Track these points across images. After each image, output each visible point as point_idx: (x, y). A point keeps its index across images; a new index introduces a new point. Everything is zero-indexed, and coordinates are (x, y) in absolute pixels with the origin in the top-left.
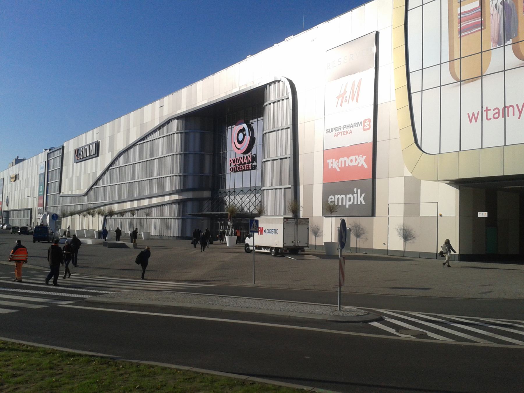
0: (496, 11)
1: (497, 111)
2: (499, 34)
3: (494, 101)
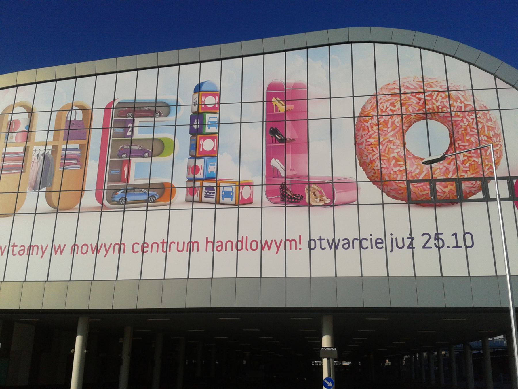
0: (36, 160)
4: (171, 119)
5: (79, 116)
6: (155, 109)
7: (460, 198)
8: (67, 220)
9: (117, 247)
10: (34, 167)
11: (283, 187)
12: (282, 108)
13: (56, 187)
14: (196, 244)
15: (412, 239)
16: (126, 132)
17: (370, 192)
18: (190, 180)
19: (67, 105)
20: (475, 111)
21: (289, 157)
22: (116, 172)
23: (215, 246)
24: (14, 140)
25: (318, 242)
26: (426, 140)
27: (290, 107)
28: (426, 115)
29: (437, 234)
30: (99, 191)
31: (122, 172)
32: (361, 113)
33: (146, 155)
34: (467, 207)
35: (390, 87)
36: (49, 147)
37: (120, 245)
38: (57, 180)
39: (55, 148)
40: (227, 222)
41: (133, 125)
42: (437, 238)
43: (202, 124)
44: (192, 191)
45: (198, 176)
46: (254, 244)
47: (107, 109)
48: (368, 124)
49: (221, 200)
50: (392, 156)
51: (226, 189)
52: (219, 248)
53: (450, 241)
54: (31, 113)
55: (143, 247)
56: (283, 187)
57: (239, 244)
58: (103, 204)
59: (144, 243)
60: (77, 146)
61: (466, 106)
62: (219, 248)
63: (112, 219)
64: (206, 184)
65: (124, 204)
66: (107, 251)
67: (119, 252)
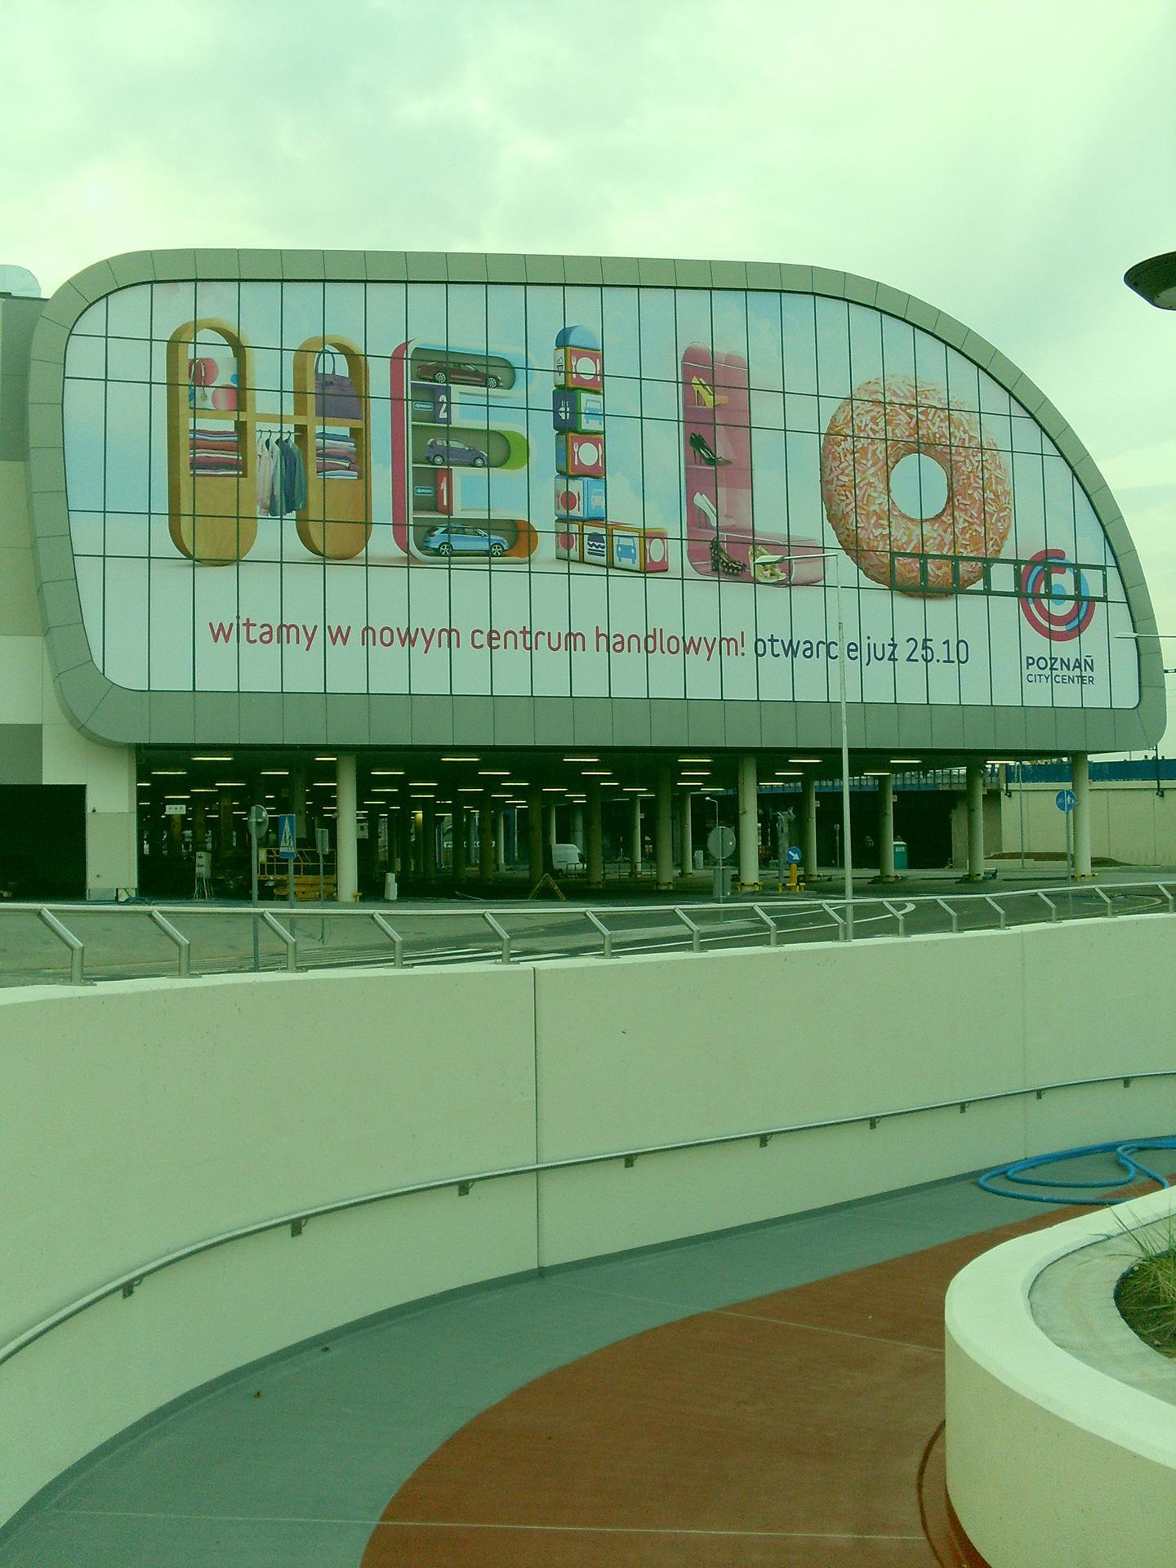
0: (266, 453)
1: (267, 629)
2: (272, 496)
3: (551, 622)
4: (516, 395)
5: (342, 368)
6: (485, 372)
7: (954, 588)
8: (345, 579)
9: (445, 635)
10: (265, 468)
11: (715, 545)
12: (708, 399)
13: (314, 513)
14: (579, 638)
15: (894, 646)
16: (436, 412)
17: (842, 568)
18: (560, 520)
19: (311, 341)
20: (981, 449)
21: (722, 492)
22: (428, 491)
23: (612, 643)
24: (209, 404)
25: (768, 644)
26: (917, 487)
27: (722, 399)
28: (921, 446)
29: (925, 640)
30: (399, 525)
31: (438, 493)
32: (830, 428)
33: (479, 462)
34: (963, 600)
35: (872, 388)
36: (289, 427)
37: (450, 632)
38: (314, 496)
39: (301, 430)
40: (628, 602)
41: (448, 398)
42: (925, 648)
43: (575, 413)
44: (565, 540)
45: (574, 513)
46: (673, 642)
47: (397, 358)
48: (839, 450)
49: (617, 563)
50: (872, 508)
51: (624, 541)
52: (619, 647)
53: (940, 652)
54: (239, 349)
55: (490, 639)
56: (715, 545)
57: (650, 642)
58: (408, 552)
59: (491, 631)
60: (345, 431)
61: (971, 438)
62: (619, 647)
63: (430, 581)
64: (589, 529)
65: (446, 554)
66: (428, 643)
67: (450, 646)
